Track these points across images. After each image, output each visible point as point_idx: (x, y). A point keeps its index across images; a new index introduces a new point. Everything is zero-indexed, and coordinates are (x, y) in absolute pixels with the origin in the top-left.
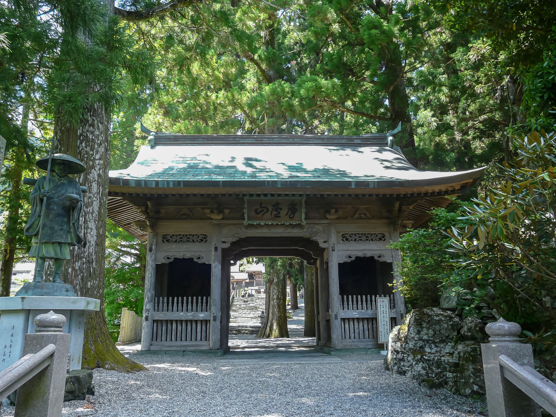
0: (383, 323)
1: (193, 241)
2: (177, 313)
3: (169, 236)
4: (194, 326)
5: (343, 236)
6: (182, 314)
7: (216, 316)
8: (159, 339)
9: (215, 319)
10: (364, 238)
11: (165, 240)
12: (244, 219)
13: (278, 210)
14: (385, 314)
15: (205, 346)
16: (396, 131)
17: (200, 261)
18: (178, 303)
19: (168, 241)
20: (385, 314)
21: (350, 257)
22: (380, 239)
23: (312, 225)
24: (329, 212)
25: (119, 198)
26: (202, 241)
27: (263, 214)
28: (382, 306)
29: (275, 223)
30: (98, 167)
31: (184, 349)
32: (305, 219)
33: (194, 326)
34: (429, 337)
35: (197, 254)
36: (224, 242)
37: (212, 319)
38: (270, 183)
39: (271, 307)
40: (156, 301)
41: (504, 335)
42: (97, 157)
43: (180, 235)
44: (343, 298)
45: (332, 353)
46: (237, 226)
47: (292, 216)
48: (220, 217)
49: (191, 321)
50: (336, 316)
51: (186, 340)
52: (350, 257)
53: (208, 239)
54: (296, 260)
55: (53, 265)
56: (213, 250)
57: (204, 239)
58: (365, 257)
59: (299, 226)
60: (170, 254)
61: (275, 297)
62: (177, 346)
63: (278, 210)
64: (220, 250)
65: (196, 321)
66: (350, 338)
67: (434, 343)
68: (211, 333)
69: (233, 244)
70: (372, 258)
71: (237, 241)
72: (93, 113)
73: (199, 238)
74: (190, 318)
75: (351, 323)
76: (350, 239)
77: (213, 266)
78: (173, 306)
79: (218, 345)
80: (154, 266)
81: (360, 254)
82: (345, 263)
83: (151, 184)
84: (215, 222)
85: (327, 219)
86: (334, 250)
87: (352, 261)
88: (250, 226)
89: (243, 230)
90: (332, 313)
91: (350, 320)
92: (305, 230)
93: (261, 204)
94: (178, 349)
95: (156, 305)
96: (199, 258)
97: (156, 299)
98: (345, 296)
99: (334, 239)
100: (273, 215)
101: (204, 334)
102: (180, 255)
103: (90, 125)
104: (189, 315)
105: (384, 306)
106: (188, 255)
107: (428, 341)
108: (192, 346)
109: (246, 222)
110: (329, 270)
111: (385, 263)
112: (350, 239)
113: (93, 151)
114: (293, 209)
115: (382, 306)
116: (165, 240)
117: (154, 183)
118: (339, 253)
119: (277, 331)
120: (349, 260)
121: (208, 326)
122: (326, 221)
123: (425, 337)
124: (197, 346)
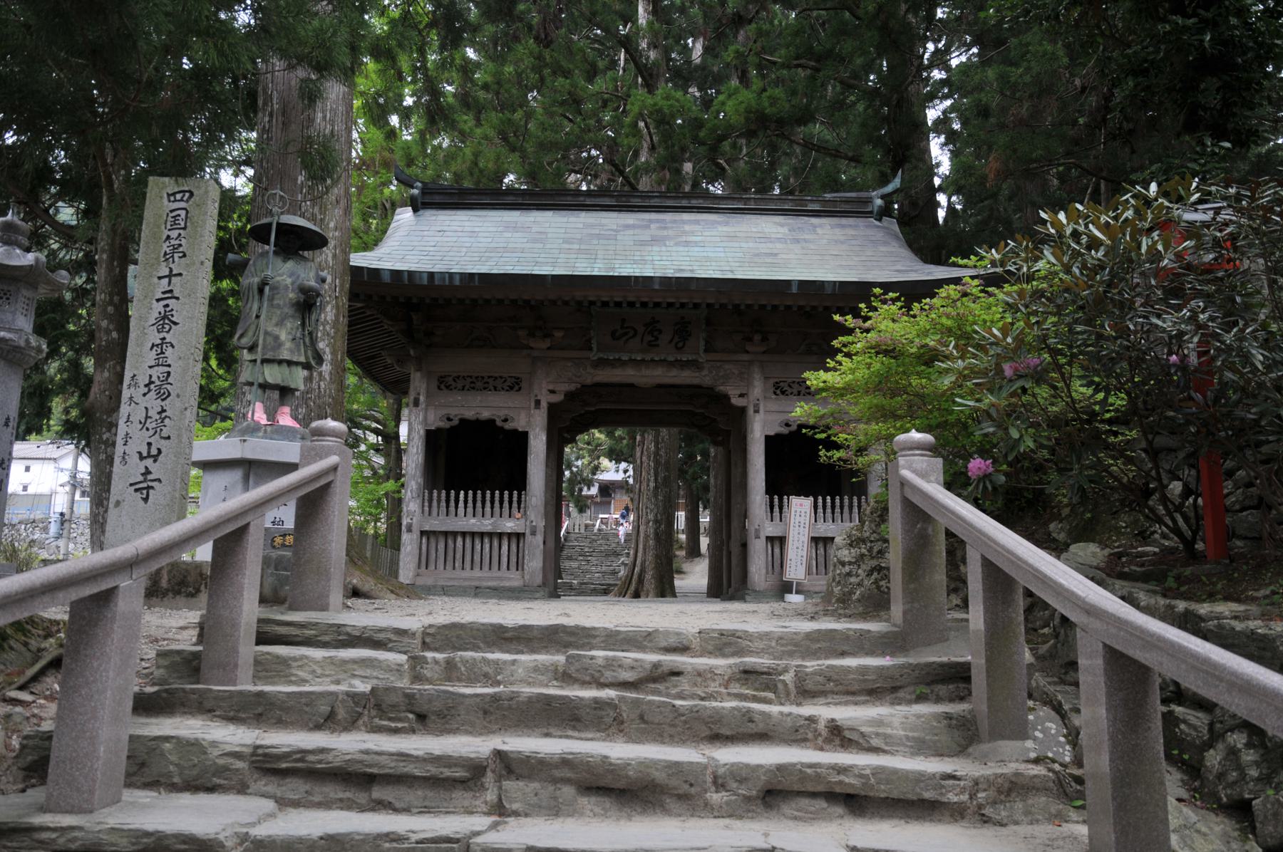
4: (496, 543)
6: (473, 521)
8: (432, 567)
12: (591, 349)
16: (889, 188)
17: (508, 426)
18: (466, 502)
19: (447, 387)
24: (750, 340)
25: (359, 305)
26: (511, 388)
29: (648, 358)
31: (477, 584)
32: (706, 351)
33: (496, 543)
35: (502, 413)
36: (552, 392)
37: (528, 532)
41: (911, 449)
47: (680, 345)
48: (547, 343)
49: (491, 535)
50: (757, 531)
56: (533, 404)
57: (514, 385)
59: (694, 365)
61: (651, 517)
62: (465, 579)
64: (544, 404)
65: (500, 535)
70: (491, 422)
74: (489, 529)
77: (531, 437)
78: (457, 507)
80: (422, 432)
82: (778, 436)
83: (421, 278)
84: (536, 353)
85: (748, 352)
86: (757, 411)
87: (791, 433)
88: (601, 363)
92: (705, 372)
93: (623, 320)
96: (506, 420)
99: (758, 389)
101: (513, 559)
102: (470, 414)
104: (486, 524)
106: (485, 414)
109: (594, 356)
112: (790, 390)
114: (683, 332)
117: (425, 276)
120: (785, 431)
122: (745, 357)
124: (500, 579)
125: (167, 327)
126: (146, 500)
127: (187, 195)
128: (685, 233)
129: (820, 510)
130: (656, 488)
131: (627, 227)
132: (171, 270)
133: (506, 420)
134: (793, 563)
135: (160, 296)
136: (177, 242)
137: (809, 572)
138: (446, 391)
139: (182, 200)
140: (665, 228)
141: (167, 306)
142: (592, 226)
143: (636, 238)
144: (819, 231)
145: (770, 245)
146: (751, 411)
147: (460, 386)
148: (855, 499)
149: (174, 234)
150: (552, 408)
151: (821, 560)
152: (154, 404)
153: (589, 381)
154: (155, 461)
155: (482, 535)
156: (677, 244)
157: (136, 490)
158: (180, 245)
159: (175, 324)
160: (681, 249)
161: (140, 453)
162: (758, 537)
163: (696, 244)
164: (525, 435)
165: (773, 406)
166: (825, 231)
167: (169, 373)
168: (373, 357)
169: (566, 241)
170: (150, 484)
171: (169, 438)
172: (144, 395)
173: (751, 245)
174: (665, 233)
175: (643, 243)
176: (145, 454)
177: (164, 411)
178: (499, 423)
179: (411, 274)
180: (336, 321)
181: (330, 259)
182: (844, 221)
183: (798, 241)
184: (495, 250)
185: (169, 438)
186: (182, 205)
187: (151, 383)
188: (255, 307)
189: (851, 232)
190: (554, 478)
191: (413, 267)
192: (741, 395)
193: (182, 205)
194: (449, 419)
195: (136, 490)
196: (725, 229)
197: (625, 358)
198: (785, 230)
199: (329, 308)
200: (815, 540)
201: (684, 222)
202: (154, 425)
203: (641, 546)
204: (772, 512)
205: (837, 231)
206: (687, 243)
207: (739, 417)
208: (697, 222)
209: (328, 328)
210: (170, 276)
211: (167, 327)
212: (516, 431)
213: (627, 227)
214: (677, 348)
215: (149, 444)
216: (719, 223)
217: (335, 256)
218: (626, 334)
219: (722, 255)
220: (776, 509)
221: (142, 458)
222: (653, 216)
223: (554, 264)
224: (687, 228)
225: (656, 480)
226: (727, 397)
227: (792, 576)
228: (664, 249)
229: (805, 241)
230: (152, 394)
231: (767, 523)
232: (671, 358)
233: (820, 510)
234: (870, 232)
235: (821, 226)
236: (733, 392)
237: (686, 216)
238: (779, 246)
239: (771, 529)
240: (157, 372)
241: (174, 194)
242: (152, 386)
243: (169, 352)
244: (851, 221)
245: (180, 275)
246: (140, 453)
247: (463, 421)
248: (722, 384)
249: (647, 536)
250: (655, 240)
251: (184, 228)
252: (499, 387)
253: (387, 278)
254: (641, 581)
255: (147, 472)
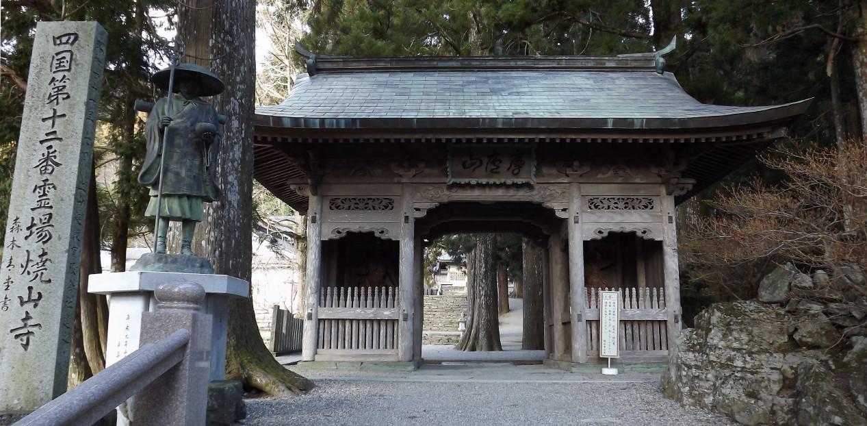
0: (608, 329)
1: (374, 208)
2: (352, 309)
3: (339, 201)
4: (376, 328)
5: (591, 202)
6: (359, 310)
7: (407, 315)
9: (405, 319)
10: (621, 205)
11: (333, 207)
13: (497, 163)
14: (612, 316)
15: (391, 355)
16: (668, 50)
17: (384, 237)
18: (353, 296)
19: (337, 208)
20: (612, 316)
21: (600, 232)
22: (646, 207)
23: (545, 186)
26: (386, 207)
27: (474, 170)
28: (608, 304)
29: (491, 181)
30: (239, 94)
31: (362, 359)
33: (376, 328)
34: (742, 345)
36: (418, 210)
37: (401, 319)
38: (487, 121)
39: (477, 306)
40: (323, 293)
42: (238, 79)
43: (355, 199)
44: (589, 293)
45: (574, 369)
46: (436, 186)
47: (516, 172)
49: (372, 321)
50: (580, 316)
51: (358, 348)
52: (600, 232)
53: (394, 205)
54: (510, 237)
55: (179, 235)
56: (403, 220)
57: (388, 205)
58: (622, 233)
59: (528, 186)
60: (341, 227)
61: (483, 293)
63: (497, 163)
64: (411, 220)
65: (379, 321)
66: (641, 349)
67: (750, 353)
68: (400, 339)
69: (430, 211)
70: (633, 234)
71: (436, 207)
72: (231, 15)
73: (383, 203)
74: (371, 316)
75: (368, 325)
76: (601, 205)
77: (402, 244)
78: (346, 300)
79: (408, 357)
80: (318, 242)
81: (616, 229)
82: (593, 241)
83: (314, 124)
85: (567, 176)
86: (576, 222)
87: (603, 238)
89: (446, 192)
90: (574, 313)
91: (382, 322)
92: (534, 193)
94: (354, 360)
95: (323, 298)
96: (382, 232)
97: (323, 290)
98: (627, 289)
99: (576, 205)
100: (489, 170)
102: (355, 228)
103: (226, 33)
105: (612, 304)
106: (366, 228)
107: (739, 350)
108: (372, 356)
110: (570, 250)
111: (652, 241)
112: (601, 205)
113: (232, 70)
115: (608, 304)
116: (333, 207)
117: (318, 121)
118: (584, 226)
119: (310, 332)
120: (599, 237)
121: (396, 329)
123: (736, 345)
125: (50, 168)
126: (26, 346)
127: (72, 37)
128: (514, 85)
129: (627, 299)
130: (486, 272)
131: (470, 83)
132: (55, 111)
133: (382, 232)
134: (607, 344)
135: (44, 137)
136: (62, 84)
137: (620, 348)
138: (336, 210)
139: (67, 43)
140: (499, 83)
141: (50, 147)
142: (443, 82)
143: (478, 90)
144: (617, 82)
145: (582, 93)
146: (571, 221)
147: (346, 206)
148: (655, 290)
149: (59, 76)
150: (418, 222)
151: (629, 337)
152: (35, 246)
153: (446, 200)
154: (35, 306)
155: (365, 321)
156: (510, 94)
157: (17, 336)
158: (64, 87)
159: (58, 165)
160: (515, 97)
161: (20, 298)
162: (580, 320)
163: (525, 93)
164: (398, 242)
165: (593, 218)
166: (621, 83)
167: (51, 215)
168: (282, 185)
169: (425, 94)
170: (31, 329)
171: (49, 281)
172: (26, 238)
173: (568, 93)
174: (500, 86)
175: (483, 94)
176: (26, 299)
177: (44, 254)
178: (377, 235)
179: (306, 120)
180: (243, 159)
181: (237, 107)
182: (634, 75)
183: (602, 89)
184: (372, 101)
185: (49, 281)
186: (68, 47)
187: (33, 225)
188: (157, 146)
189: (641, 82)
190: (419, 272)
191: (309, 115)
192: (564, 210)
193: (68, 47)
194: (339, 232)
195: (17, 336)
196: (545, 82)
197: (473, 181)
198: (591, 82)
199: (236, 148)
200: (624, 322)
201: (513, 78)
202: (35, 269)
203: (476, 313)
204: (624, 301)
205: (632, 82)
206: (518, 93)
207: (560, 226)
208: (523, 78)
209: (236, 164)
210: (53, 117)
211: (50, 168)
212: (390, 240)
213: (470, 83)
214: (513, 173)
215: (30, 288)
216: (540, 78)
217: (241, 105)
218: (473, 164)
219: (547, 101)
220: (593, 298)
221: (22, 303)
222: (489, 74)
223: (418, 110)
224: (516, 82)
225: (486, 267)
226: (552, 211)
227: (606, 354)
228: (500, 97)
229: (609, 89)
230: (34, 236)
231: (587, 311)
232: (509, 182)
233: (627, 299)
234: (658, 82)
235: (618, 78)
236: (557, 206)
237: (514, 74)
238: (589, 93)
239: (590, 315)
240: (40, 214)
241: (59, 38)
242: (34, 229)
243: (51, 193)
244: (639, 74)
245: (64, 115)
246: (20, 298)
247: (349, 233)
248: (549, 201)
249: (480, 306)
250: (494, 92)
251: (69, 70)
252: (377, 207)
253: (288, 124)
254: (476, 338)
255: (28, 317)
